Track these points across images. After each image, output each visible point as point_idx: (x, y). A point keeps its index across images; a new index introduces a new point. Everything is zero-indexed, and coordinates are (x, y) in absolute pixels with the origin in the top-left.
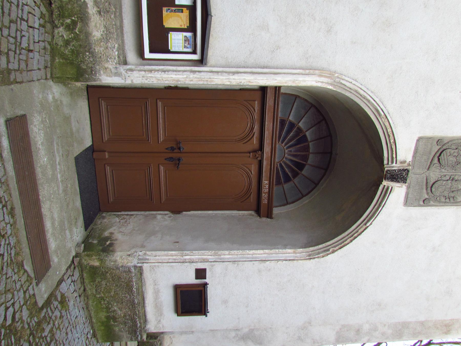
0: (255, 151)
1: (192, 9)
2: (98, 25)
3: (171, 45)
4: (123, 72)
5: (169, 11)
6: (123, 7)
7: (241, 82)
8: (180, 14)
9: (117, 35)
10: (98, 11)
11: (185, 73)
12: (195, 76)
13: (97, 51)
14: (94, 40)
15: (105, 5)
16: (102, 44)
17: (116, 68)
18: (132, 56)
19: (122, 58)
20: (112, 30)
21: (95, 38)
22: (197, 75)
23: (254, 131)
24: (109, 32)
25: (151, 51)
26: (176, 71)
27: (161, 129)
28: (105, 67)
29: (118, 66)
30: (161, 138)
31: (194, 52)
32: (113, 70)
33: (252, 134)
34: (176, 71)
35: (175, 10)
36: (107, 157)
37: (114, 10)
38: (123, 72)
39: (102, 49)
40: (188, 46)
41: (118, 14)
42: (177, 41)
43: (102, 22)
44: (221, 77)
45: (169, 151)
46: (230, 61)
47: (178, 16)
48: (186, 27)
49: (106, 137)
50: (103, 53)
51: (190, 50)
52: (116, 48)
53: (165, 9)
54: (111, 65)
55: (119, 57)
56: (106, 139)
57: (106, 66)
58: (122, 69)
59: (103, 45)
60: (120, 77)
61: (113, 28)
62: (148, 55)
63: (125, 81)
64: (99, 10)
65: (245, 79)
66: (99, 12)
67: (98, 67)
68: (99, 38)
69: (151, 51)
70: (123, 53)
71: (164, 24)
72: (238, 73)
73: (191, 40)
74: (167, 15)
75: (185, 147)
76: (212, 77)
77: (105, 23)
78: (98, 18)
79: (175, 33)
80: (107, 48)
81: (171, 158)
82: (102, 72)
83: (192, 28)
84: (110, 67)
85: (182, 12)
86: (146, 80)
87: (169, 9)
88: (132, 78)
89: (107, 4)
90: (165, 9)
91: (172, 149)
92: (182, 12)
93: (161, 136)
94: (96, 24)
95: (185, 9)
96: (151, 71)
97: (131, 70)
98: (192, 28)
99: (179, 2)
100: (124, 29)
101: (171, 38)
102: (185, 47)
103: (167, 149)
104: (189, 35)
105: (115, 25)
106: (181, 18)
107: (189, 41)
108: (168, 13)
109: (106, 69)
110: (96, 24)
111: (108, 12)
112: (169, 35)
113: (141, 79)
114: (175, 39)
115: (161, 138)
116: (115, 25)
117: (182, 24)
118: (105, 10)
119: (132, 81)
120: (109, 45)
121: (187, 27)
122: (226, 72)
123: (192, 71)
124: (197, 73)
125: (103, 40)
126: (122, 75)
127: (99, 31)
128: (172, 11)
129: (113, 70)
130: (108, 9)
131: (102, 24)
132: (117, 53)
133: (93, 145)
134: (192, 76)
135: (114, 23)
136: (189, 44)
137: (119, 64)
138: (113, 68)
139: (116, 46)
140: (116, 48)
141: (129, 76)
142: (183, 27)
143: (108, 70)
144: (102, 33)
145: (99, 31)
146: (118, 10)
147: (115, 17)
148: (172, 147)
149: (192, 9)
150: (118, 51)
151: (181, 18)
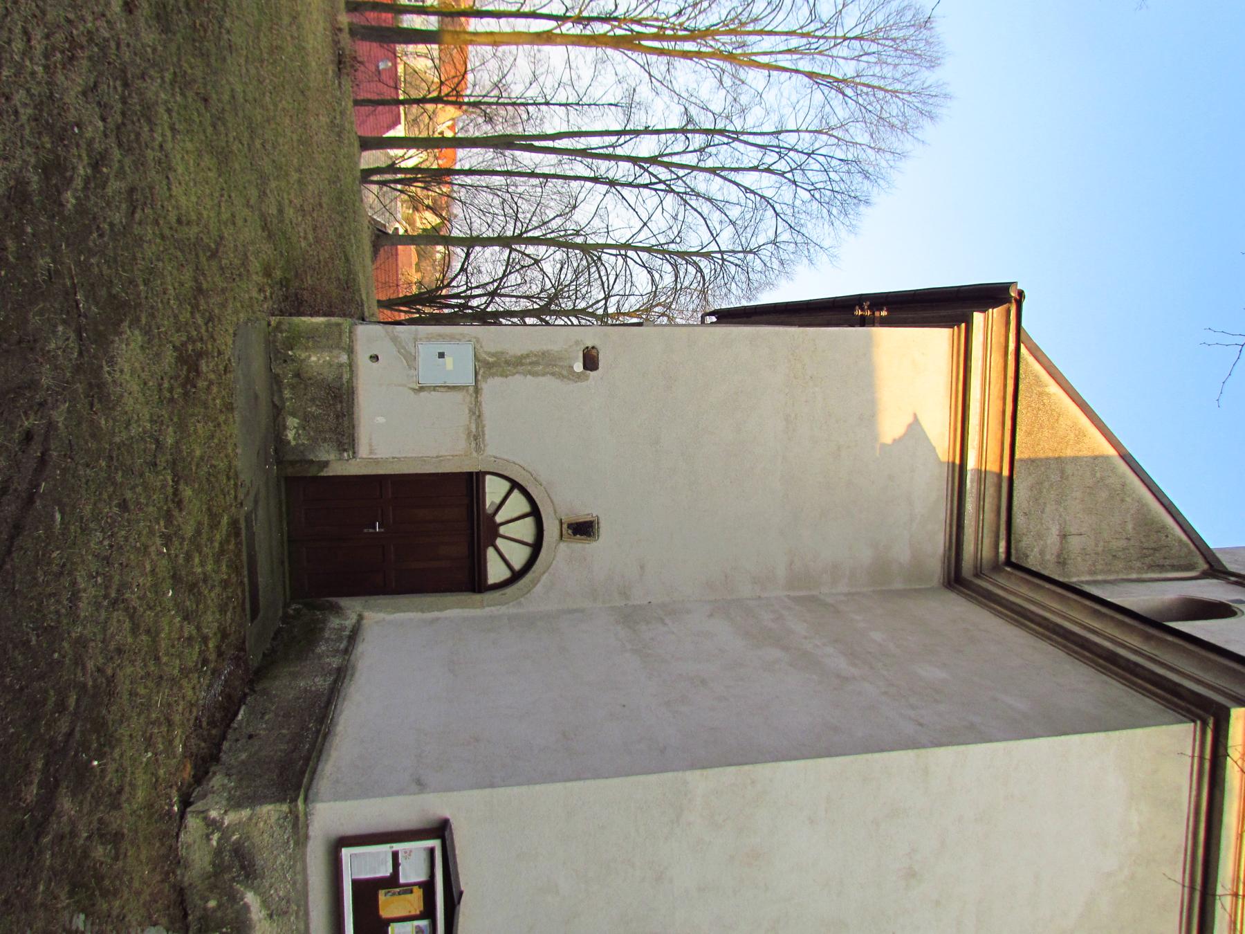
8: (409, 896)
53: (381, 893)
83: (428, 912)
98: (428, 912)
104: (423, 923)
128: (394, 894)
142: (413, 913)
147: (297, 917)
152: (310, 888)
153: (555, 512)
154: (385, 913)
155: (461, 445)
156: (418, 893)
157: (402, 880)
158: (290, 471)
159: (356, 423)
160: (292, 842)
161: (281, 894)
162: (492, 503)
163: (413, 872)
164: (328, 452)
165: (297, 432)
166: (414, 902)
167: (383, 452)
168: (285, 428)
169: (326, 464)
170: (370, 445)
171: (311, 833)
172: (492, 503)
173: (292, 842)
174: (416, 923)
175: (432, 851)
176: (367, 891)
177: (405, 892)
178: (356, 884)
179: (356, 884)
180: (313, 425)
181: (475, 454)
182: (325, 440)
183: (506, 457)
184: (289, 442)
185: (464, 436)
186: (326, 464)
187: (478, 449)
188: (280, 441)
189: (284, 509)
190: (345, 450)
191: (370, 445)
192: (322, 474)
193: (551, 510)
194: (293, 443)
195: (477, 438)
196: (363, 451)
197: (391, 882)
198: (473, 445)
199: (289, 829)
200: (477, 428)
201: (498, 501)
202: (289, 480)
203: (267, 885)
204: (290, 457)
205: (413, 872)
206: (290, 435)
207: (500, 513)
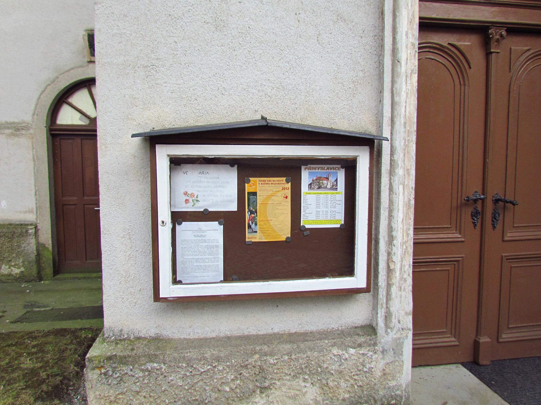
0: (486, 43)
1: (247, 168)
2: (292, 392)
3: (330, 222)
4: (393, 334)
5: (253, 226)
6: (246, 333)
7: (413, 45)
8: (260, 199)
9: (311, 349)
10: (261, 392)
11: (395, 186)
12: (400, 162)
13: (347, 396)
14: (323, 400)
15: (248, 378)
16: (331, 384)
17: (383, 352)
18: (355, 313)
19: (362, 339)
20: (301, 361)
21: (319, 398)
22: (399, 156)
23: (445, 44)
24: (306, 367)
25: (349, 271)
26: (391, 211)
27: (438, 236)
28: (381, 377)
29: (379, 348)
30: (456, 236)
31: (350, 167)
32: (389, 358)
33: (452, 49)
34: (391, 211)
35: (252, 212)
36: (488, 340)
37: (257, 356)
38: (393, 334)
39: (343, 384)
40: (332, 179)
41: (265, 348)
42: (322, 209)
43: (284, 385)
44: (403, 94)
45: (479, 220)
46: (361, 74)
47: (265, 204)
48: (289, 185)
49: (449, 340)
50: (352, 381)
51: (341, 176)
52: (341, 352)
53: (250, 237)
54: (378, 364)
55: (360, 346)
56: (453, 339)
57: (378, 373)
58: (385, 338)
59: (334, 381)
60: (403, 342)
61: (297, 359)
62: (358, 280)
63: (409, 330)
64: (258, 391)
65: (407, 35)
66: (263, 389)
67: (381, 393)
68: (318, 391)
69: (349, 271)
70: (350, 335)
71: (284, 239)
72: (394, 51)
73: (320, 171)
74: (263, 232)
75: (473, 189)
76: (402, 120)
77: (288, 377)
78: (278, 393)
79: (302, 213)
80: (341, 372)
81: (494, 218)
82: (393, 383)
83: (290, 169)
84: (381, 364)
85: (255, 194)
86: (405, 280)
87: (250, 227)
88: (403, 313)
89: (245, 373)
90: (250, 237)
91: (474, 215)
92: (255, 194)
93: (450, 236)
94: (289, 397)
95: (248, 188)
96: (389, 271)
97: (388, 317)
98: (290, 169)
99: (231, 201)
100: (293, 331)
101: (314, 222)
102: (334, 187)
103: (475, 225)
104: (306, 177)
105: (289, 354)
106: (269, 197)
107: (319, 179)
108: (257, 228)
109: (385, 374)
110: (289, 397)
111: (262, 369)
112: (307, 226)
113: (403, 293)
114: (318, 212)
115: (456, 236)
116: (289, 354)
117: (281, 194)
118: (258, 377)
119: (407, 314)
120: (333, 367)
121: (287, 182)
122: (393, 82)
123: (391, 173)
124: (396, 157)
125: (324, 382)
126: (399, 339)
127: (305, 390)
128: (253, 220)
129: (389, 358)
130: (257, 370)
131: (289, 383)
132: (352, 351)
133: (464, 364)
134: (400, 172)
135: (287, 358)
136: (327, 179)
137: (375, 344)
138: (383, 358)
139: (335, 351)
140: (341, 352)
141: (399, 322)
142: (288, 193)
143: (387, 371)
144: (308, 385)
145: (305, 390)
146: (258, 348)
147: (272, 354)
148: (472, 216)
149: (247, 168)
150: (346, 347)
151: (269, 197)
152: (236, 333)
153: (81, 67)
154: (283, 232)
155: (24, 141)
156: (256, 184)
157: (233, 207)
158: (49, 270)
159: (7, 223)
160: (149, 366)
161: (231, 377)
162: (80, 119)
163: (219, 190)
164: (29, 244)
165: (14, 266)
166: (272, 193)
167: (31, 203)
168: (10, 275)
169: (40, 247)
170: (26, 212)
171: (153, 332)
172: (80, 119)
173: (149, 366)
174: (304, 188)
175: (176, 162)
176: (243, 258)
177: (253, 203)
178: (229, 276)
179: (229, 276)
180: (7, 254)
181: (32, 131)
182: (19, 246)
183: (33, 106)
184: (22, 272)
185: (16, 139)
186: (40, 247)
187: (27, 127)
188: (21, 278)
189: (81, 275)
190: (27, 231)
191: (26, 212)
192: (50, 248)
193: (80, 70)
194: (22, 269)
195: (17, 129)
196: (31, 218)
197: (234, 224)
198: (23, 132)
199: (125, 369)
200: (8, 128)
201: (78, 115)
202: (57, 271)
203: (214, 395)
204: (34, 271)
205: (219, 190)
206: (16, 271)
207: (89, 113)
